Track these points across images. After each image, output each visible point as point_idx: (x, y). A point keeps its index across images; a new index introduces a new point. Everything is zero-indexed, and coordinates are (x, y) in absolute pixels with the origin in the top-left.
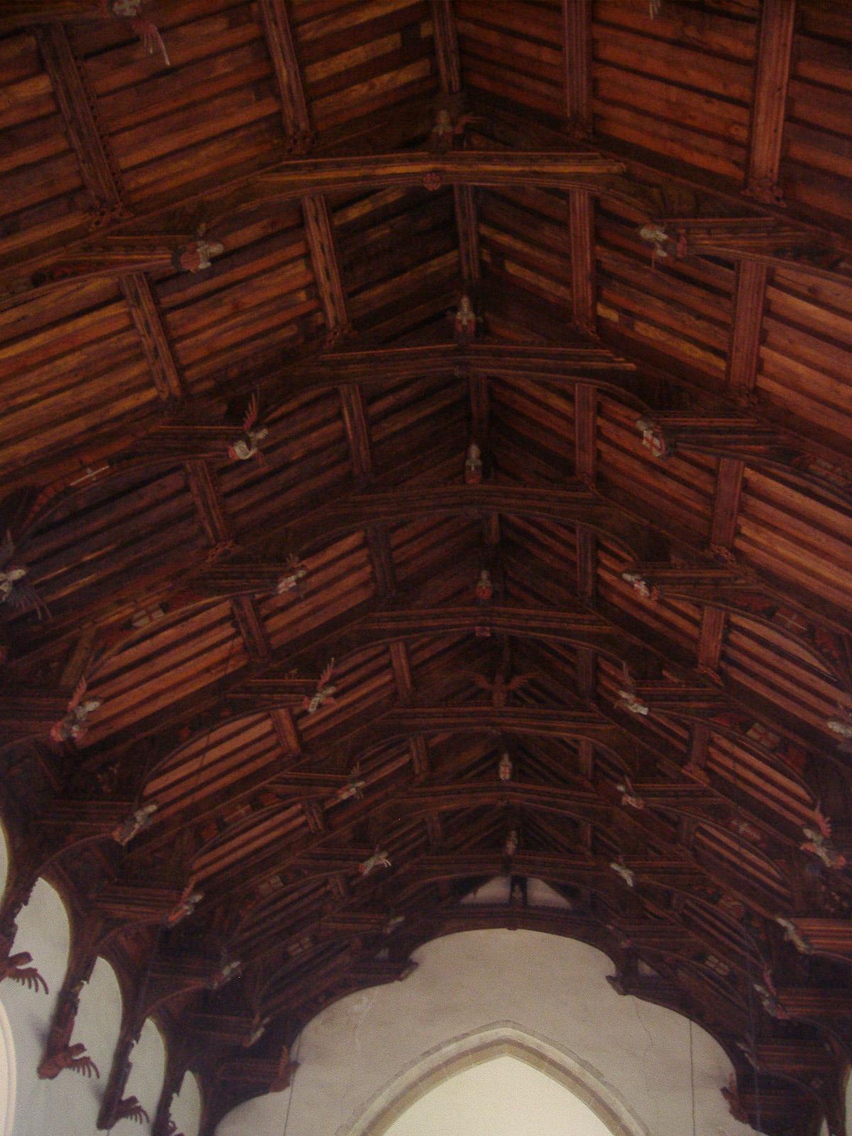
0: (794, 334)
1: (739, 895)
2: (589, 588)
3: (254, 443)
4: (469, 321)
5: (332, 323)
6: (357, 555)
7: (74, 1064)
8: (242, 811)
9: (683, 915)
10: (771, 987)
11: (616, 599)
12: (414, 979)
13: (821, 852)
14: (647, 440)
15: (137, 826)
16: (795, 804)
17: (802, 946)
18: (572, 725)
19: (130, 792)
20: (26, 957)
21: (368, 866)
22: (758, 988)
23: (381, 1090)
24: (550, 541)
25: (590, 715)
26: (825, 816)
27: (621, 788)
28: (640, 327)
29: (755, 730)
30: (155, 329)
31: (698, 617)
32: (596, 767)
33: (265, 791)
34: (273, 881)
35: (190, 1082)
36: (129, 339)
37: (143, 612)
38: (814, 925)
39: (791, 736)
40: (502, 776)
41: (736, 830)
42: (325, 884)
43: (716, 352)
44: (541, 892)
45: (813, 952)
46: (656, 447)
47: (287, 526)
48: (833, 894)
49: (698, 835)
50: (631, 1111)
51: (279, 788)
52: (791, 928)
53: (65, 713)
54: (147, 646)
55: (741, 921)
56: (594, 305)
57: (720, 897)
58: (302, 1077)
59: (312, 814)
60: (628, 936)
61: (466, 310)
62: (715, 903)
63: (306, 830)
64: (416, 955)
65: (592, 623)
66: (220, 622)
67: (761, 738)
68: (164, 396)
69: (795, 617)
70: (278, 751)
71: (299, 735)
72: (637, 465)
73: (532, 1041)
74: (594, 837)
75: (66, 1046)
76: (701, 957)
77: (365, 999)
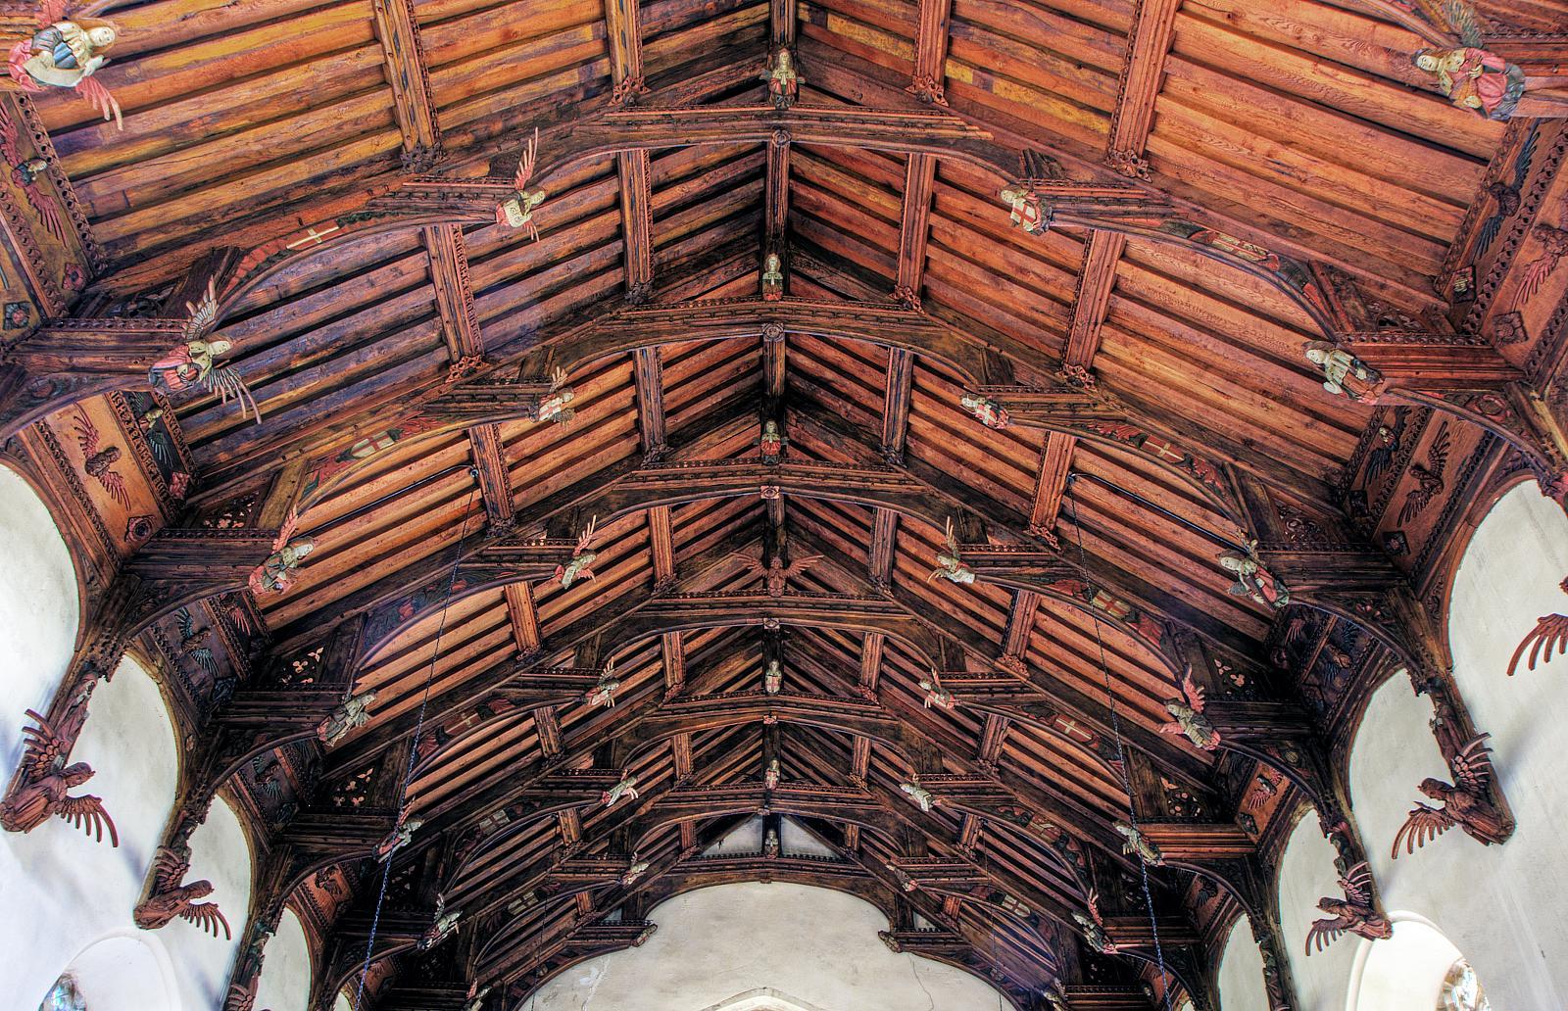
0: (1201, 74)
2: (897, 441)
3: (528, 206)
4: (789, 81)
5: (620, 74)
6: (621, 395)
9: (976, 851)
10: (1096, 916)
11: (929, 454)
12: (653, 943)
14: (1017, 211)
15: (349, 721)
17: (1148, 857)
18: (863, 616)
19: (336, 679)
20: (204, 887)
21: (612, 798)
22: (1079, 919)
24: (851, 387)
25: (883, 604)
28: (999, 86)
30: (407, 44)
31: (1034, 466)
32: (882, 674)
33: (495, 696)
34: (496, 817)
36: (371, 57)
37: (366, 441)
38: (1161, 831)
39: (1140, 603)
40: (769, 688)
41: (1061, 729)
42: (556, 823)
43: (1098, 112)
44: (797, 839)
45: (1160, 863)
46: (1029, 218)
47: (546, 343)
49: (1006, 747)
51: (513, 692)
52: (1133, 835)
54: (364, 493)
55: (1055, 845)
56: (943, 63)
57: (1030, 819)
59: (546, 732)
60: (913, 878)
61: (784, 67)
62: (1024, 825)
63: (537, 753)
65: (901, 482)
66: (456, 468)
68: (410, 145)
69: (1167, 446)
70: (512, 647)
71: (540, 626)
72: (975, 273)
74: (871, 765)
76: (997, 897)
77: (594, 971)
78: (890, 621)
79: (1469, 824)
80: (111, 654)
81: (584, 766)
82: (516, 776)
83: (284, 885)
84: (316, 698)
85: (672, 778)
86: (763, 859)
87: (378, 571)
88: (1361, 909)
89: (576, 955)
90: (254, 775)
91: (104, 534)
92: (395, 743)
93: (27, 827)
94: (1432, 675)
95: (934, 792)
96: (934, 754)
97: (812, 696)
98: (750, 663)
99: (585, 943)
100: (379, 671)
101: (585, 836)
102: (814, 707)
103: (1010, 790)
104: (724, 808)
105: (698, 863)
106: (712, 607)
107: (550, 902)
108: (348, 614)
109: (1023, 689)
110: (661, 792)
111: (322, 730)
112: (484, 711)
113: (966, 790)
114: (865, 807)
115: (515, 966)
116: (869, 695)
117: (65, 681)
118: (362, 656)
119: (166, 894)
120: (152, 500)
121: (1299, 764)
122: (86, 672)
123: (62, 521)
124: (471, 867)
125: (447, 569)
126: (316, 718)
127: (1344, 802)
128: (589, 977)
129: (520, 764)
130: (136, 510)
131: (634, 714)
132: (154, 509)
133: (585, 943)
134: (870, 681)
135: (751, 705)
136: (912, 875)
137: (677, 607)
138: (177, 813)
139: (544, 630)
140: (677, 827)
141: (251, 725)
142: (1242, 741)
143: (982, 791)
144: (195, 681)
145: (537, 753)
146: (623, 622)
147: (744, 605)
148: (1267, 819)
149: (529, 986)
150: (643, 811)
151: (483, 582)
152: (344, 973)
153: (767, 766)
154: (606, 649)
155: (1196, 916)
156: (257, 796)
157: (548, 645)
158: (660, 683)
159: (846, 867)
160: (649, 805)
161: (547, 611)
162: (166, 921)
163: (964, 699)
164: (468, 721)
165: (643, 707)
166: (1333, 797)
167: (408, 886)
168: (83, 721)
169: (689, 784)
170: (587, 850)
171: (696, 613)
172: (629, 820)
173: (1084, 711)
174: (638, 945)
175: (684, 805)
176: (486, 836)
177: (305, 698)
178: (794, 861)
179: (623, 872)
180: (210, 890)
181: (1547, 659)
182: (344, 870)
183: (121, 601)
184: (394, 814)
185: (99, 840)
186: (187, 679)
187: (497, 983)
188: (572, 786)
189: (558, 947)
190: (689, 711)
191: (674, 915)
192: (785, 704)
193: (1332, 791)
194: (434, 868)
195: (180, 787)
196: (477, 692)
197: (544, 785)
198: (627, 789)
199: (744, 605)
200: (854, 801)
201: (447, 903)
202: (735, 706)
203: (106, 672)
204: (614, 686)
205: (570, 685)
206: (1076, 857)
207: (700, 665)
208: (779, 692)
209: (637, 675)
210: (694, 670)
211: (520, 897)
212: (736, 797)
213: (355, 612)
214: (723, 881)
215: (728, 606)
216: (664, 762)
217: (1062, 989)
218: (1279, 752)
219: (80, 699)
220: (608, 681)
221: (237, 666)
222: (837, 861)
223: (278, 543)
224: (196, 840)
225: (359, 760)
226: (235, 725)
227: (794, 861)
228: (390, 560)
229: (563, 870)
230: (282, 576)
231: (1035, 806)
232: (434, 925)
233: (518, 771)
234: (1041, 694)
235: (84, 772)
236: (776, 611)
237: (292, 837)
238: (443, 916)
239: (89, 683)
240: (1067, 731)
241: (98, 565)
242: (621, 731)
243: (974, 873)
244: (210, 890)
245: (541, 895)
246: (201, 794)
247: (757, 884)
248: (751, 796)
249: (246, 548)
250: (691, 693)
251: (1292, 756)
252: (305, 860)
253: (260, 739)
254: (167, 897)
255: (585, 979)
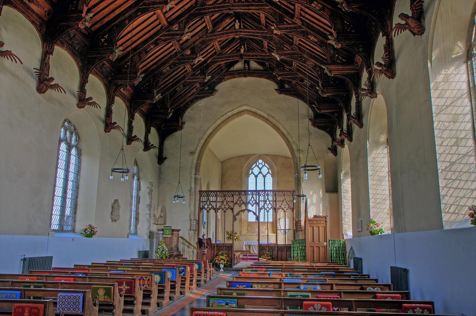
1: (312, 60)
7: (114, 128)
8: (152, 47)
10: (321, 87)
12: (217, 94)
13: (333, 43)
15: (117, 54)
16: (326, 27)
17: (329, 74)
19: (112, 43)
20: (91, 98)
21: (196, 61)
22: (317, 88)
23: (210, 127)
26: (335, 31)
27: (273, 28)
29: (314, 4)
32: (266, 22)
33: (158, 39)
34: (167, 69)
35: (153, 130)
39: (325, 4)
40: (236, 28)
41: (309, 39)
42: (185, 68)
44: (254, 65)
45: (332, 76)
48: (340, 57)
50: (283, 127)
51: (163, 38)
52: (326, 68)
53: (82, 18)
55: (313, 68)
58: (185, 126)
59: (176, 45)
60: (280, 76)
62: (305, 63)
63: (175, 51)
64: (217, 88)
67: (316, 6)
70: (160, 26)
71: (167, 19)
73: (253, 110)
74: (268, 46)
75: (111, 123)
76: (302, 80)
77: (203, 102)
78: (264, 9)
79: (386, 74)
80: (51, 49)
81: (188, 54)
82: (171, 58)
83: (114, 93)
84: (108, 49)
85: (215, 52)
86: (244, 71)
87: (117, 12)
88: (372, 91)
89: (198, 99)
90: (99, 68)
91: (40, 17)
92: (134, 54)
93: (44, 92)
94: (387, 32)
95: (280, 55)
96: (281, 44)
97: (248, 29)
98: (232, 19)
99: (200, 96)
100: (125, 37)
101: (194, 70)
102: (249, 32)
103: (302, 53)
104: (230, 60)
105: (227, 73)
106: (214, 8)
107: (187, 88)
108: (112, 25)
109: (300, 27)
110: (213, 57)
111: (110, 57)
112: (156, 44)
113: (289, 54)
114: (268, 57)
115: (182, 103)
116: (264, 28)
117: (42, 57)
118: (117, 36)
119: (83, 101)
120: (49, 6)
121: (362, 52)
122: (47, 54)
123: (27, 17)
124: (161, 83)
125: (136, 9)
126: (108, 55)
127: (372, 62)
128: (201, 103)
129: (171, 54)
130: (46, 9)
131: (200, 38)
132: (50, 8)
133: (200, 96)
134: (263, 24)
135: (232, 33)
136: (280, 75)
137: (204, 9)
138: (81, 82)
139: (169, 20)
140: (220, 65)
141: (93, 58)
142: (347, 46)
143: (294, 54)
144: (77, 48)
145: (175, 51)
146: (190, 15)
147: (223, 7)
148: (360, 63)
149: (187, 107)
150: (208, 62)
151: (146, 12)
152: (136, 109)
153: (241, 47)
154: (186, 23)
155: (348, 87)
156: (102, 73)
157: (171, 23)
158: (206, 29)
159: (267, 71)
160: (210, 60)
161: (168, 15)
162: (84, 107)
163: (283, 31)
164: (152, 47)
165: (202, 36)
166: (370, 61)
167: (147, 88)
168: (49, 66)
169: (220, 54)
170: (195, 73)
171: (210, 10)
172: (205, 65)
173: (316, 33)
174: (213, 95)
175: (219, 60)
176: (165, 74)
177: (105, 50)
178: (252, 71)
179: (204, 78)
180: (92, 99)
181: (398, 35)
182: (130, 86)
183: (50, 34)
184: (136, 73)
185: (61, 93)
186: (75, 48)
187: (179, 107)
188: (186, 59)
189: (193, 97)
190: (215, 36)
191: (222, 87)
192: (241, 32)
193: (369, 59)
194: (153, 83)
195: (80, 75)
196: (155, 39)
197: (178, 59)
198: (200, 59)
199: (223, 7)
200: (264, 56)
201: (157, 92)
202: (227, 33)
203: (51, 53)
204: (189, 34)
205: (177, 35)
206: (318, 71)
207: (217, 22)
208: (239, 29)
209: (199, 28)
210: (216, 23)
211: (179, 86)
212: (233, 56)
213: (114, 24)
214: (234, 78)
215: (219, 7)
216: (213, 49)
217: (317, 104)
218: (357, 49)
219: (47, 61)
220: (187, 33)
221: (86, 43)
222: (264, 71)
223: (83, 15)
224: (87, 87)
225: (126, 60)
226: (90, 58)
227: (252, 71)
228: (120, 9)
229: (189, 79)
230: (87, 23)
231: (308, 58)
232: (154, 97)
233: (171, 56)
234: (304, 28)
235: (52, 79)
236: (232, 8)
237: (113, 81)
238: (156, 95)
239: (48, 57)
240: (311, 39)
241: (41, 25)
242: (197, 43)
243: (296, 74)
244: (92, 99)
245: (184, 86)
246: (86, 76)
247: (243, 78)
248: (237, 56)
249: (76, 16)
250: (215, 30)
251: (361, 49)
252: (118, 86)
253: (96, 61)
254: (83, 101)
255: (201, 104)
